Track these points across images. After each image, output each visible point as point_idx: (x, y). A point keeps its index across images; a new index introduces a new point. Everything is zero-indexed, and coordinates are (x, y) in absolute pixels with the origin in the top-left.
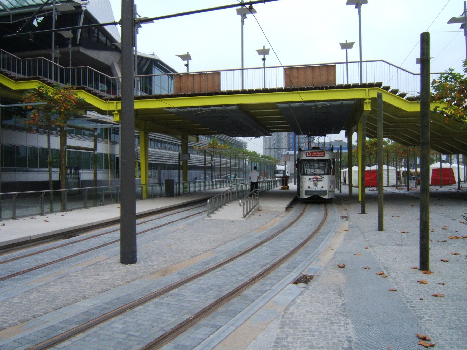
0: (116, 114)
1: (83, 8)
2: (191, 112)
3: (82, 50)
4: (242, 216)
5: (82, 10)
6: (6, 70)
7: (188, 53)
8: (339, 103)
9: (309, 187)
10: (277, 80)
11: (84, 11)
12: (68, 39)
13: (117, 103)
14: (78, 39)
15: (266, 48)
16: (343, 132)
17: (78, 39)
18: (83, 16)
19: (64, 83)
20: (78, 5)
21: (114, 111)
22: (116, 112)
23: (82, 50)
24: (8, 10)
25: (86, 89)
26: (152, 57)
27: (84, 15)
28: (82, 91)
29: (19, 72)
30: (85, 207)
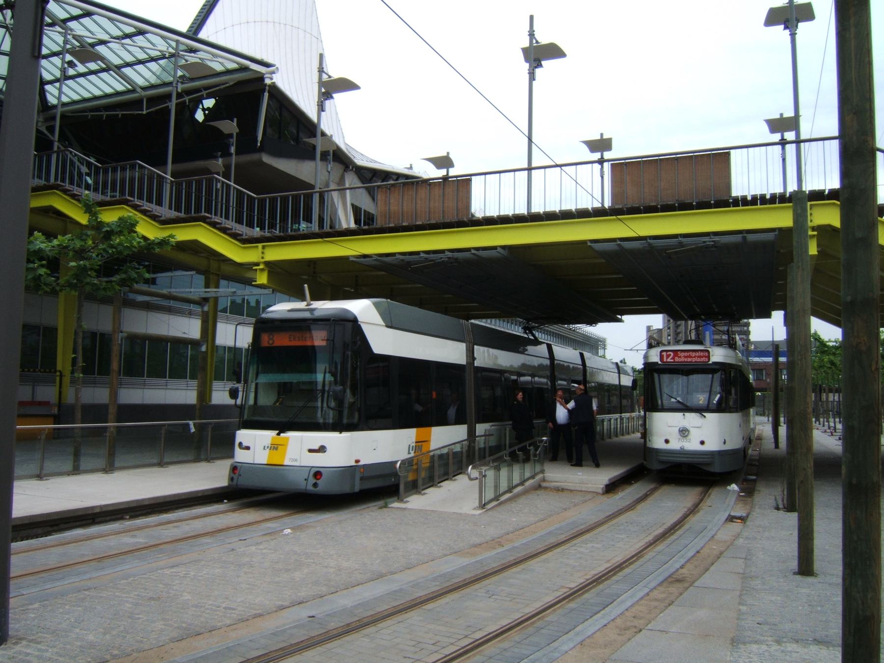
0: (262, 270)
1: (268, 81)
2: (409, 263)
3: (267, 159)
4: (477, 504)
5: (266, 85)
6: (76, 188)
7: (448, 153)
8: (738, 238)
9: (667, 441)
10: (591, 189)
11: (270, 86)
12: (231, 136)
13: (264, 247)
14: (260, 138)
15: (605, 137)
16: (778, 316)
17: (260, 138)
18: (266, 95)
19: (253, 228)
20: (259, 75)
21: (257, 264)
22: (261, 266)
23: (267, 159)
24: (139, 90)
25: (208, 220)
26: (406, 172)
27: (269, 92)
28: (123, 208)
29: (250, 225)
30: (161, 464)
